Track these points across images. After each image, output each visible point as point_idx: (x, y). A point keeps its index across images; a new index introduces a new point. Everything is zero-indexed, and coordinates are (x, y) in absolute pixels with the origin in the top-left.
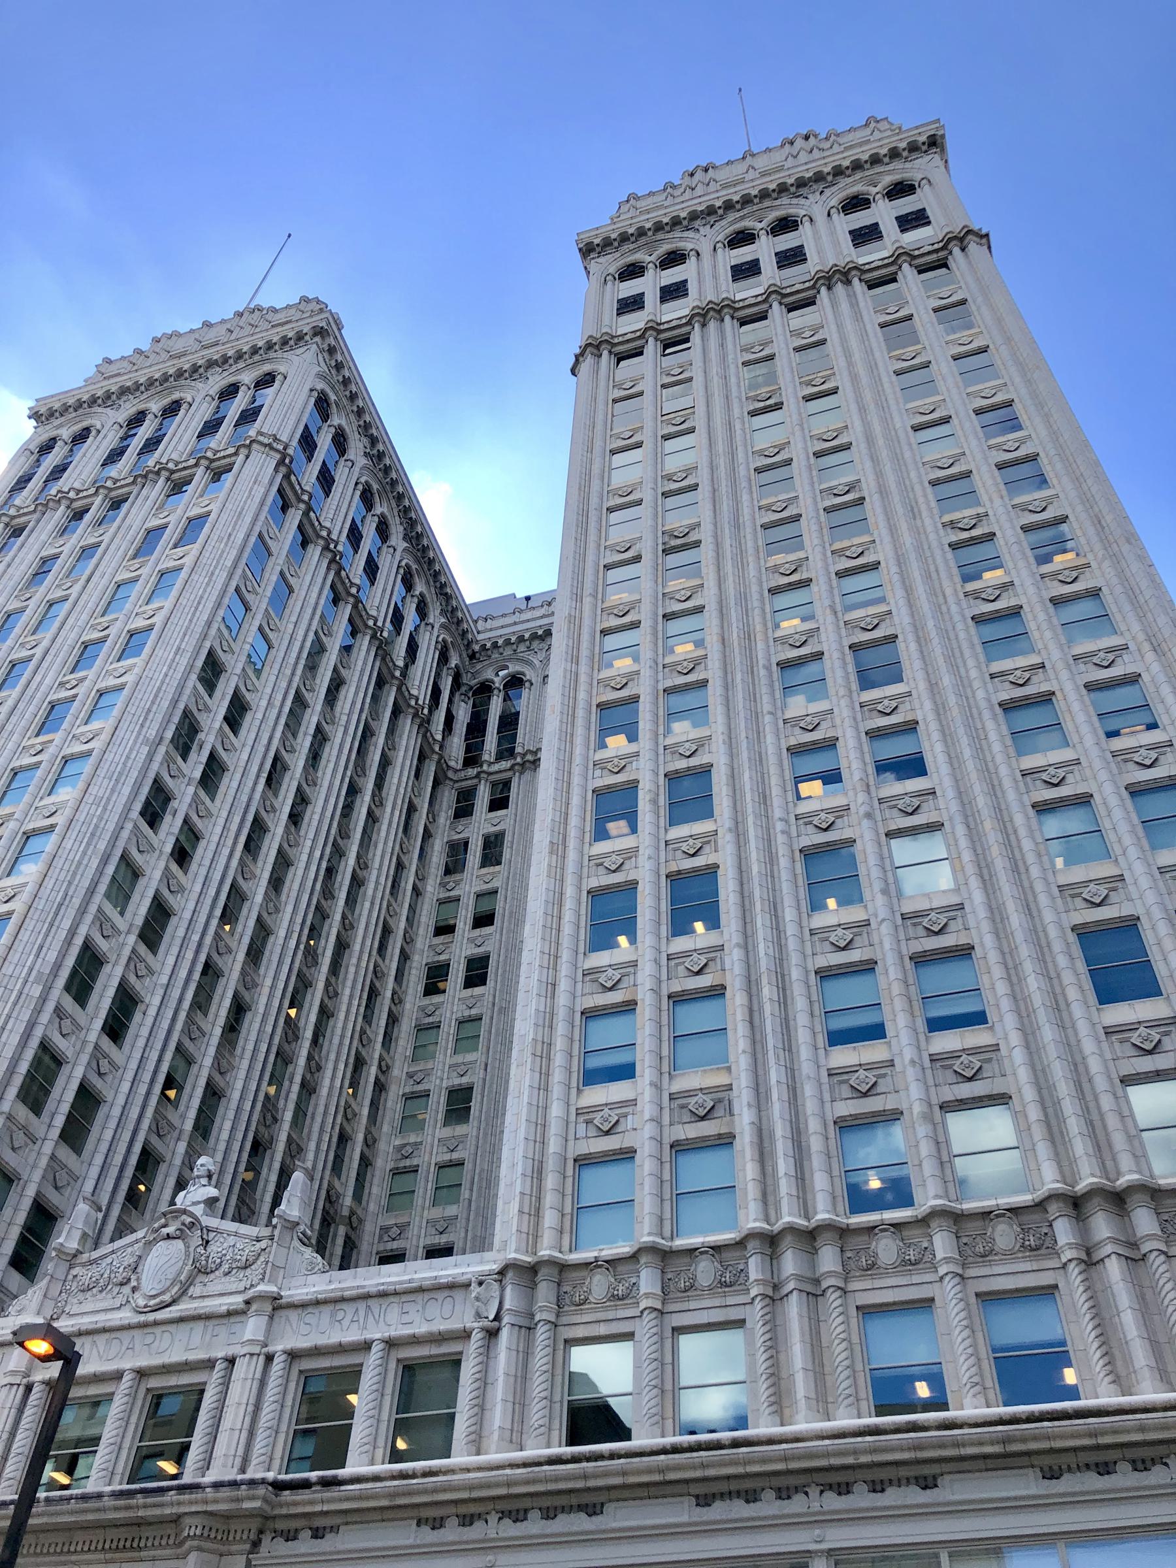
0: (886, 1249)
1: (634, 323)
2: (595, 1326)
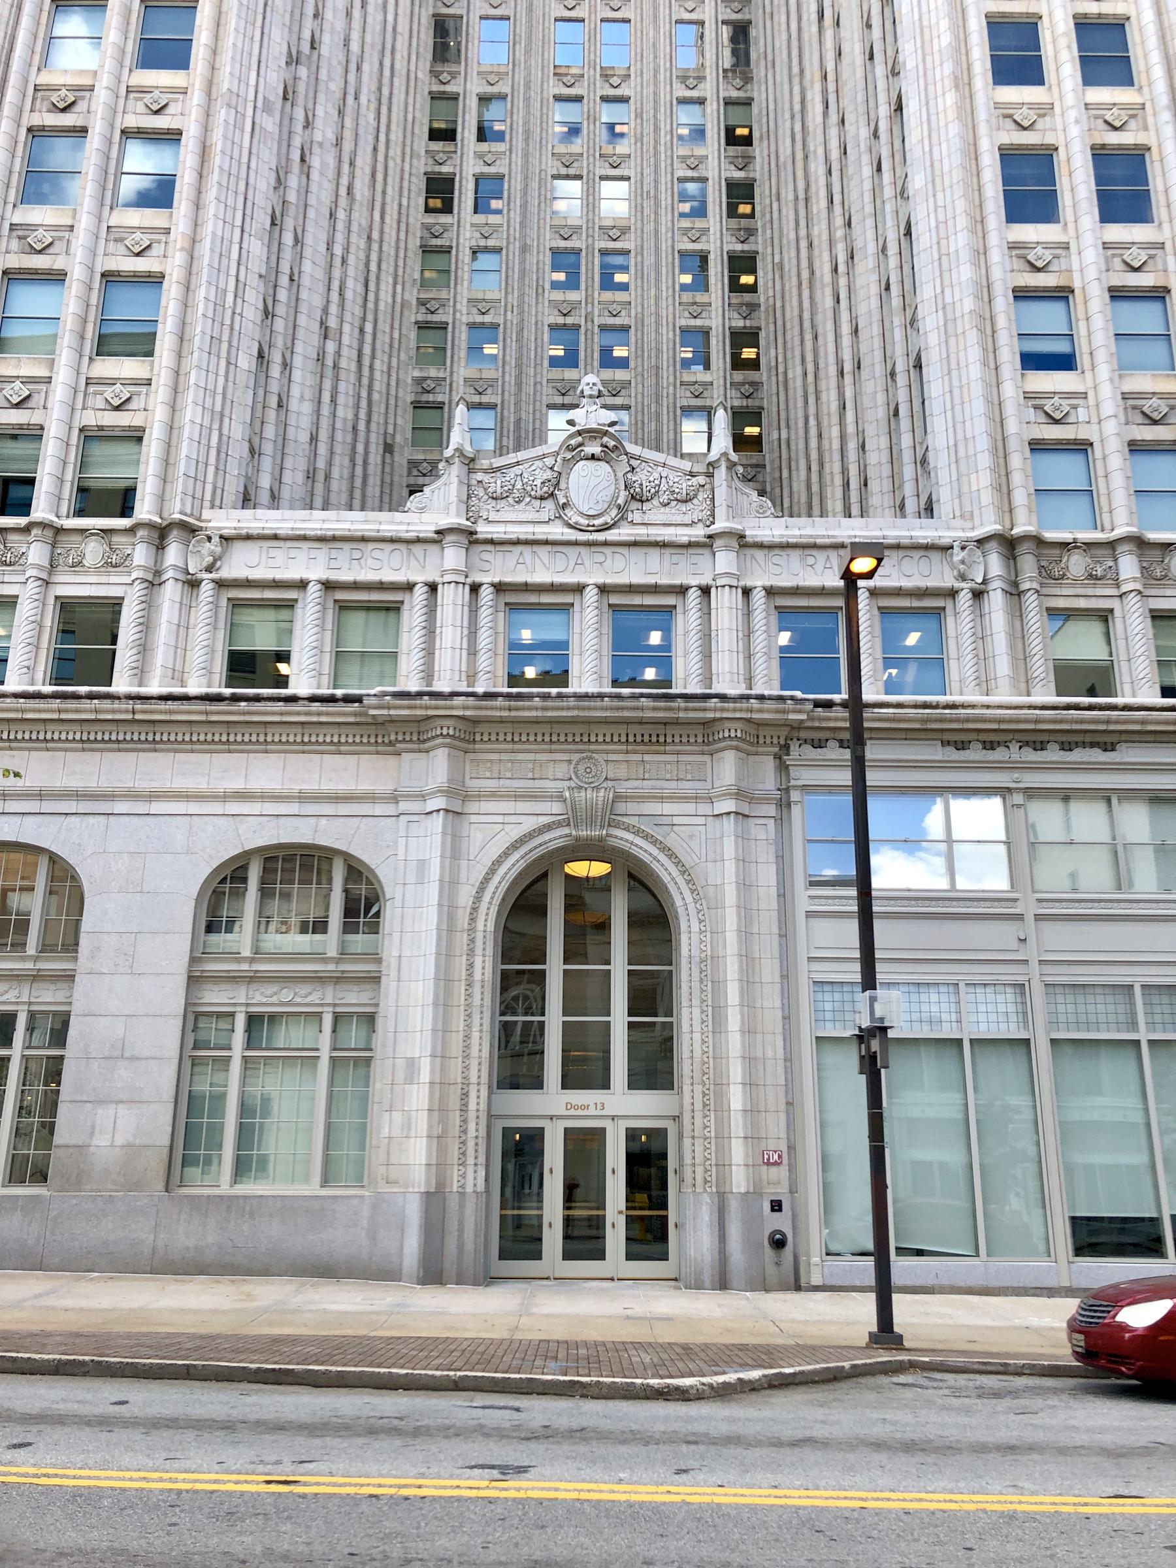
2: (1076, 599)
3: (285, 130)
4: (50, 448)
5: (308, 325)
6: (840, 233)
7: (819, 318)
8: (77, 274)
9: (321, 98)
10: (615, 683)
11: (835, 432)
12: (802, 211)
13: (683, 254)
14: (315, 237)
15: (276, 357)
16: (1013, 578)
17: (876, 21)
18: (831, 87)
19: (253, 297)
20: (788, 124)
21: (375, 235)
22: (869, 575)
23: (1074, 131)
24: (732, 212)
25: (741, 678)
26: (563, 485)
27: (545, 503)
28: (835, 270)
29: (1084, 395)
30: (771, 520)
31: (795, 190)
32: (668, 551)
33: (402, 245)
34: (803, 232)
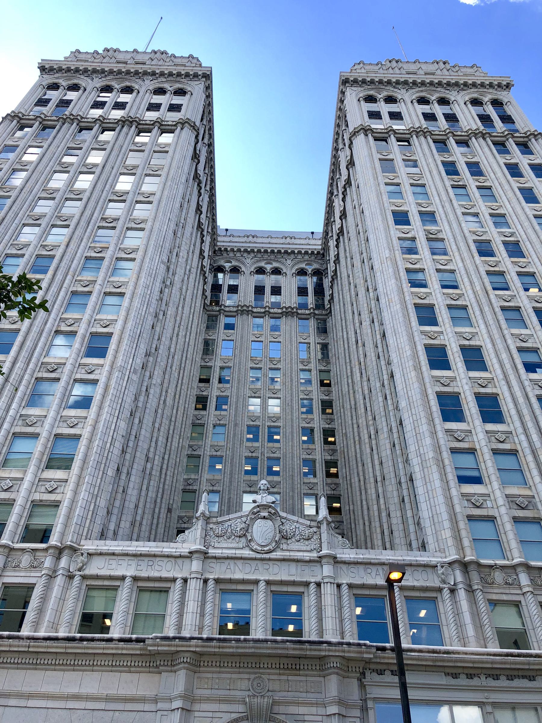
0: (498, 576)
1: (151, 116)
3: (141, 380)
4: (16, 509)
5: (140, 456)
6: (371, 423)
7: (364, 457)
8: (44, 434)
9: (157, 368)
10: (274, 633)
11: (375, 507)
12: (354, 413)
13: (303, 428)
14: (148, 420)
15: (125, 470)
16: (468, 583)
17: (380, 345)
18: (363, 367)
19: (118, 445)
20: (346, 380)
21: (173, 419)
22: (400, 580)
23: (466, 387)
24: (324, 412)
25: (338, 633)
26: (250, 531)
27: (241, 539)
28: (370, 437)
29: (489, 495)
30: (348, 550)
31: (350, 404)
32: (300, 564)
33: (184, 423)
34: (355, 421)
